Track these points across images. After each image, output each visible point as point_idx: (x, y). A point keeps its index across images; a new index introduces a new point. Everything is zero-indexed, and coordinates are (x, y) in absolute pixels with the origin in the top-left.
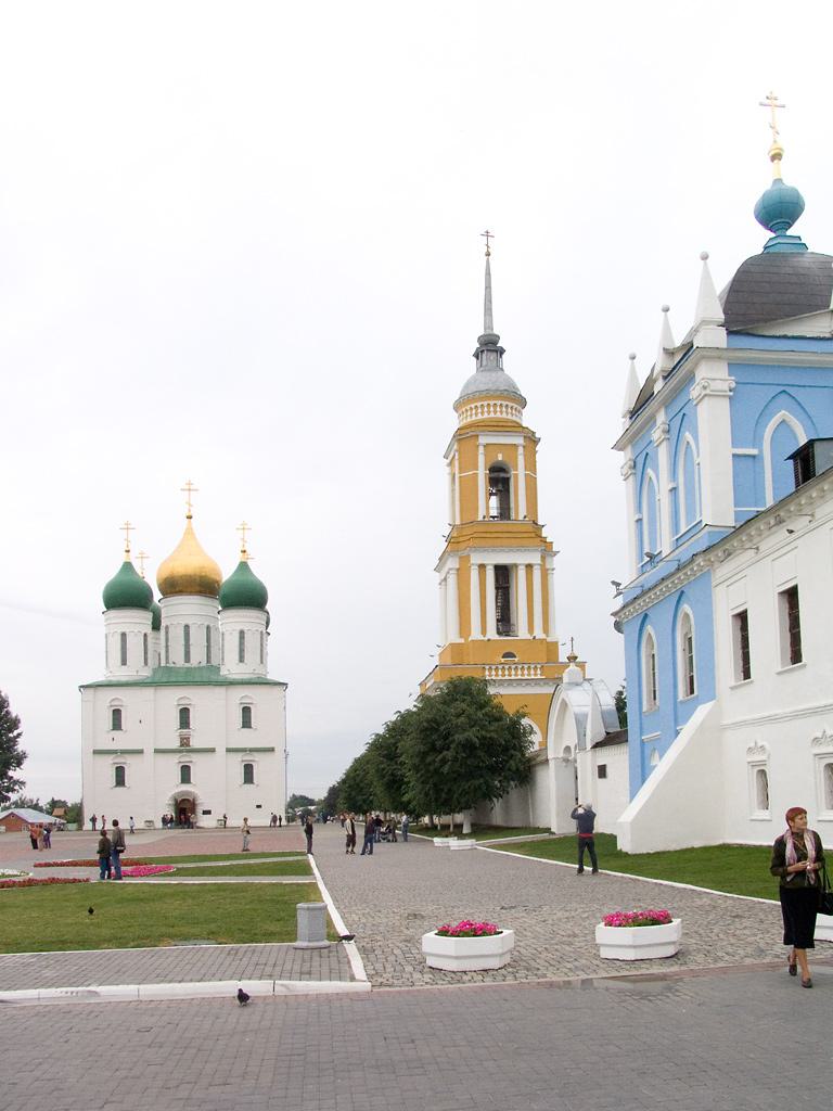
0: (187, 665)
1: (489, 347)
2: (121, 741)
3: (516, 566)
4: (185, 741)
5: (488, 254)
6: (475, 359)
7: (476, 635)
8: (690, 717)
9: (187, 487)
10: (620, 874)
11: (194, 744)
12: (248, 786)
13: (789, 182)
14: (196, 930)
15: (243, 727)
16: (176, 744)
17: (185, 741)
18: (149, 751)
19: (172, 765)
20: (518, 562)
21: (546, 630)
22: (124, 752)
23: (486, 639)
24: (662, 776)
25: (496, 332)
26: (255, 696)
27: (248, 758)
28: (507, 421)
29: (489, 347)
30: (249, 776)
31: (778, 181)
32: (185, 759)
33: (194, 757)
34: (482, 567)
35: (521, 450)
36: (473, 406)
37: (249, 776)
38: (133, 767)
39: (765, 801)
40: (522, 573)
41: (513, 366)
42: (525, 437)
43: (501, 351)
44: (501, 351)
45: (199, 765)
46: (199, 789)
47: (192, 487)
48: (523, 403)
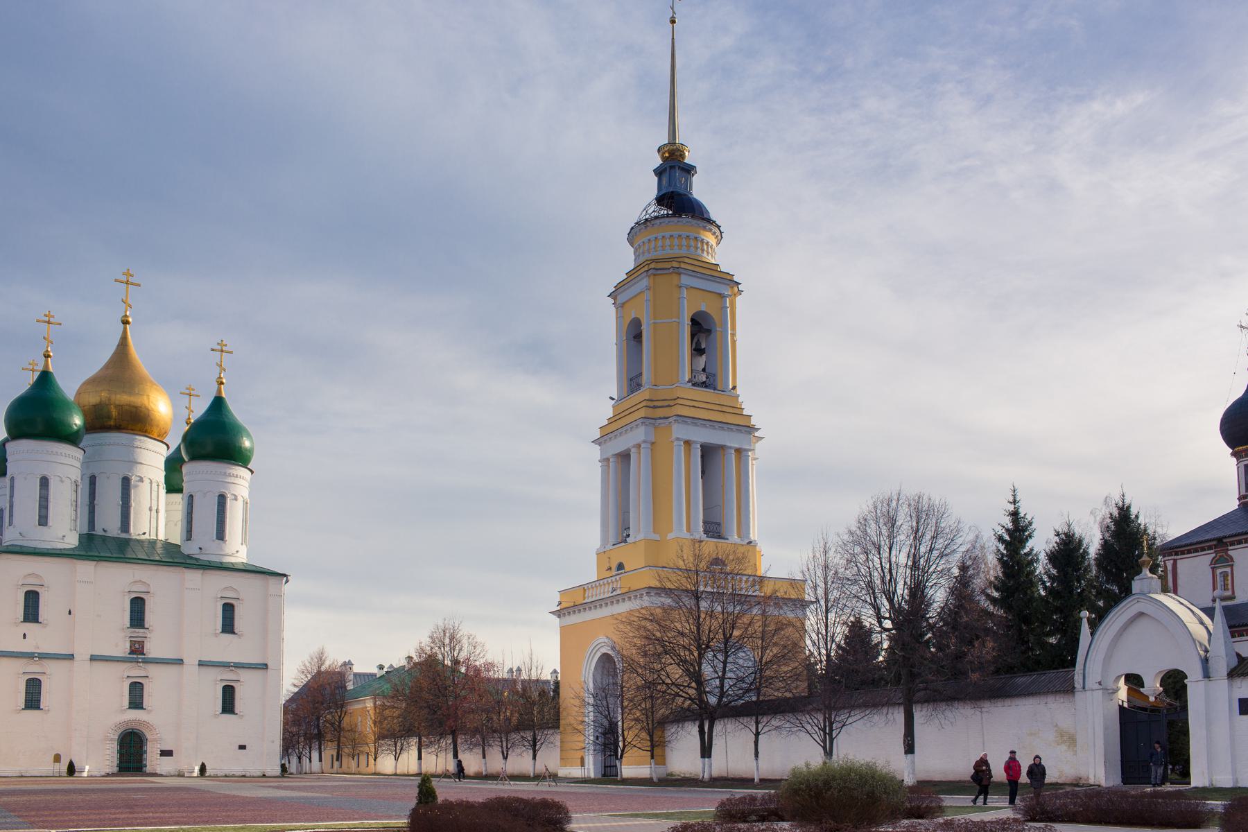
0: (124, 536)
2: (39, 638)
3: (723, 447)
4: (137, 650)
5: (673, 22)
9: (124, 278)
11: (154, 649)
12: (228, 717)
14: (1068, 789)
15: (224, 631)
16: (123, 649)
17: (137, 650)
19: (114, 683)
20: (728, 444)
22: (44, 657)
26: (246, 591)
27: (229, 676)
30: (228, 702)
32: (136, 672)
33: (153, 670)
36: (660, 235)
37: (228, 702)
38: (54, 681)
39: (191, 497)
45: (158, 684)
46: (158, 720)
47: (131, 280)
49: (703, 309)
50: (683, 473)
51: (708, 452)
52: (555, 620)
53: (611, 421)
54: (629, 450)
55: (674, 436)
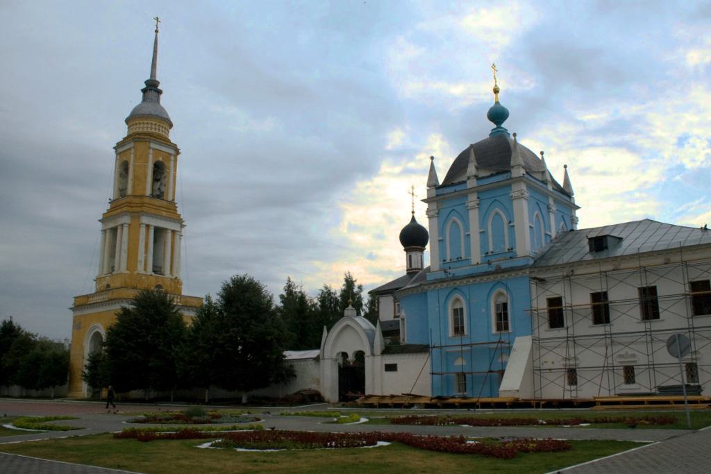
1: (152, 88)
5: (157, 31)
6: (142, 94)
7: (140, 269)
8: (364, 376)
10: (569, 468)
13: (502, 104)
18: (686, 403)
21: (171, 273)
23: (173, 278)
24: (619, 430)
25: (157, 79)
28: (159, 135)
29: (152, 88)
31: (497, 103)
34: (148, 226)
40: (169, 235)
41: (167, 102)
43: (160, 92)
44: (160, 92)
48: (171, 125)
51: (159, 232)
52: (71, 312)
53: (109, 211)
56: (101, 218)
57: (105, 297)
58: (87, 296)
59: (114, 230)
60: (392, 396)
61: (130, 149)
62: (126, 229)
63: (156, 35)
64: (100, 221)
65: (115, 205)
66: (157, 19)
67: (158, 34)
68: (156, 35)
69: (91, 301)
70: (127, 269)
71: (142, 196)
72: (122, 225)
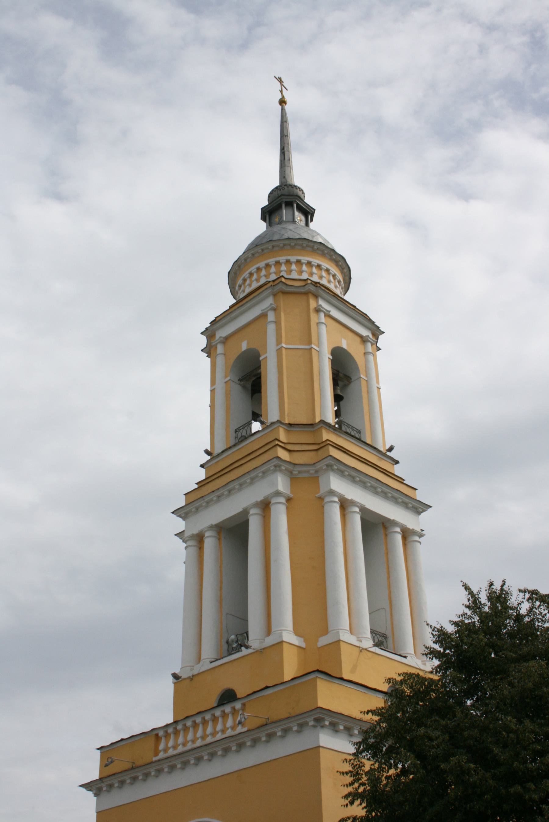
34: (345, 505)
35: (271, 316)
42: (275, 295)
49: (244, 346)
50: (343, 542)
51: (375, 528)
52: (90, 798)
53: (201, 484)
54: (245, 513)
55: (323, 490)
56: (93, 773)
57: (228, 726)
58: (154, 735)
59: (235, 533)
60: (379, 388)
61: (264, 315)
62: (280, 518)
63: (283, 109)
64: (87, 786)
65: (224, 469)
66: (280, 80)
67: (287, 107)
68: (283, 109)
69: (170, 747)
70: (297, 632)
71: (312, 427)
72: (265, 506)
